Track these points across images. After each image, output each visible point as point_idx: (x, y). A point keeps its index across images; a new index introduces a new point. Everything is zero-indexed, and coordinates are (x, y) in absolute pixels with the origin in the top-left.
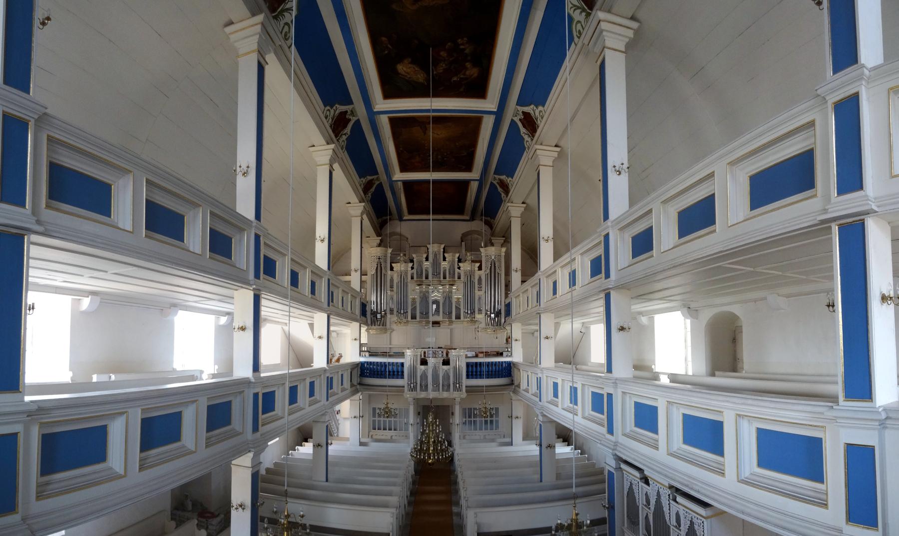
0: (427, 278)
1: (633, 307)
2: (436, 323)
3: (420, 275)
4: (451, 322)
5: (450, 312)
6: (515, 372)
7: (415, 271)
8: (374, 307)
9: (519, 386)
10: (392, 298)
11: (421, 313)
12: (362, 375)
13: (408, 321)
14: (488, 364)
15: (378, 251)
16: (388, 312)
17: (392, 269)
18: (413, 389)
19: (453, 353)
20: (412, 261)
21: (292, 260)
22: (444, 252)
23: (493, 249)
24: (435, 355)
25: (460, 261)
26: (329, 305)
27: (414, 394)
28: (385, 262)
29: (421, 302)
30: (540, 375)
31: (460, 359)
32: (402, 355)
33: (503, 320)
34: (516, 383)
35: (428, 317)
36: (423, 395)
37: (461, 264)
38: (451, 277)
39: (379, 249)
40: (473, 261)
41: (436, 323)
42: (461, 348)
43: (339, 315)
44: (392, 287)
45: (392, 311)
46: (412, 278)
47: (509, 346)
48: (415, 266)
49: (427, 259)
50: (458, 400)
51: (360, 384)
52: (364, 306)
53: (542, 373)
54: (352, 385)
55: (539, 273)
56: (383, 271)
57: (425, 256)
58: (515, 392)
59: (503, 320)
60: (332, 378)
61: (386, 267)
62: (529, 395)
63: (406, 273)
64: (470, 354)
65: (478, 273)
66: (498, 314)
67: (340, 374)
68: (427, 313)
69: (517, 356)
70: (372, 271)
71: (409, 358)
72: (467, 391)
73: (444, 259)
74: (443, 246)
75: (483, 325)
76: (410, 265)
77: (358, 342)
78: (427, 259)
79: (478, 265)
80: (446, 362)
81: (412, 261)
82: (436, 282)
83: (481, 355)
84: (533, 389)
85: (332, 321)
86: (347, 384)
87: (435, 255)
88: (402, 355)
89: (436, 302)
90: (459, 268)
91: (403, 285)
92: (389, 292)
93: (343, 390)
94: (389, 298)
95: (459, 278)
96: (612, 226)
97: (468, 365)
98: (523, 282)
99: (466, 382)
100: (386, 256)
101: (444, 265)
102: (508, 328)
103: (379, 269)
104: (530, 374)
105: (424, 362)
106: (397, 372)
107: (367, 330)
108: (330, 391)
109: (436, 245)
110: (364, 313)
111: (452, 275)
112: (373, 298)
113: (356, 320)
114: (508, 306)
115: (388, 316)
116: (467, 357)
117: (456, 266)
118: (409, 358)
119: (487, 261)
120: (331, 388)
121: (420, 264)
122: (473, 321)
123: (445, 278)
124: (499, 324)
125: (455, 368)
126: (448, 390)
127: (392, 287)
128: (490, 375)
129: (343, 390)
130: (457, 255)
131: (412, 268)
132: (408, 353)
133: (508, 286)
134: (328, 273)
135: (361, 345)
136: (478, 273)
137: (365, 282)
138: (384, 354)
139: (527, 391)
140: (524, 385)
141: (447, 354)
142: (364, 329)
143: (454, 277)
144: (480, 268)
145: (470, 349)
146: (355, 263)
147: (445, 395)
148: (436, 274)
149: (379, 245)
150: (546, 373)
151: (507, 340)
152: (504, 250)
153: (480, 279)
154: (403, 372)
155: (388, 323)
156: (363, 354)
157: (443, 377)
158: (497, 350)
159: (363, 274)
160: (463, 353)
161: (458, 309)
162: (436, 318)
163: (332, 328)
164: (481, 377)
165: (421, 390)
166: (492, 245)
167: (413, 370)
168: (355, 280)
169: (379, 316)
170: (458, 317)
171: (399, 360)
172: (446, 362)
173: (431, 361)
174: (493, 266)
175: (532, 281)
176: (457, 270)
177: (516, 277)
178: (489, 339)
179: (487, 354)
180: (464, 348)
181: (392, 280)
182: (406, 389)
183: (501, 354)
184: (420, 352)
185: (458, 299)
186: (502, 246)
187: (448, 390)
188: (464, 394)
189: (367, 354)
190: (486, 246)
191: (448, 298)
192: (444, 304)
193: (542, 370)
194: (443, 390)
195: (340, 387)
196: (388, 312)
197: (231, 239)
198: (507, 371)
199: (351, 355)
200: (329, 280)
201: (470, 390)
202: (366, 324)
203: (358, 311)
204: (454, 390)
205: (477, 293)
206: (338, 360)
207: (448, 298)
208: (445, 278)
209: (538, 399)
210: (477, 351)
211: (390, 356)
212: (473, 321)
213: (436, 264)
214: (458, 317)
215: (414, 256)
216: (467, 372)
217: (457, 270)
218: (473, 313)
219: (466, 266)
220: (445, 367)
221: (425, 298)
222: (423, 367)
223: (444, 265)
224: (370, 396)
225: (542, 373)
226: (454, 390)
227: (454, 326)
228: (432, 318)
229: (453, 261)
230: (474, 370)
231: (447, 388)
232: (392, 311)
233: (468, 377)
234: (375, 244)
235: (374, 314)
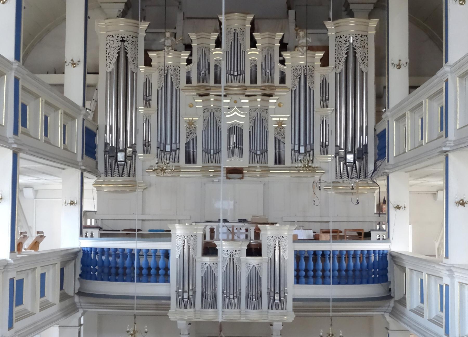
0: (218, 81)
1: (410, 182)
2: (235, 172)
3: (204, 75)
4: (266, 170)
5: (262, 149)
6: (393, 273)
7: (193, 67)
8: (111, 138)
9: (403, 301)
10: (147, 122)
11: (206, 151)
12: (86, 274)
13: (178, 169)
14: (340, 255)
15: (122, 26)
16: (140, 147)
17: (148, 62)
18: (185, 303)
19: (267, 232)
20: (188, 47)
21: (47, 103)
22: (253, 30)
23: (352, 22)
24: (232, 236)
25: (284, 47)
26: (16, 132)
27: (189, 313)
28: (135, 48)
29: (206, 129)
30: (446, 281)
31: (283, 243)
32: (166, 235)
33: (371, 167)
34: (397, 296)
35: (218, 160)
36: (209, 315)
37: (286, 55)
38: (265, 81)
39: (122, 22)
40: (310, 48)
41: (235, 172)
42: (285, 222)
43: (37, 153)
44: (147, 99)
45: (147, 146)
46: (189, 81)
47: (383, 218)
48: (195, 58)
49: (218, 44)
50: (278, 326)
51: (80, 293)
52: (90, 136)
53: (451, 276)
54: (64, 297)
55: (446, 68)
56: (131, 67)
57: (214, 37)
58: (395, 313)
59: (371, 167)
60: (20, 282)
61: (136, 58)
62: (424, 321)
63: (177, 70)
64: (303, 234)
65: (319, 73)
66: (361, 154)
67: (39, 272)
68: (218, 152)
69: (400, 240)
70: (106, 66)
71: (180, 241)
72: (296, 310)
73: (253, 44)
74: (250, 18)
75: (331, 176)
76: (185, 55)
77: (77, 209)
78: (218, 44)
79: (320, 55)
80: (254, 251)
81: (188, 47)
82: (236, 91)
83: (324, 237)
84: (433, 308)
85: (22, 164)
86: (53, 293)
87: (235, 36)
88: (166, 235)
89: (235, 130)
90: (282, 62)
91: (170, 97)
92: (141, 109)
93: (45, 306)
94: (141, 120)
95: (282, 81)
96: (452, 72)
97: (298, 256)
98: (412, 88)
99: (295, 291)
100: (136, 36)
101: (253, 55)
102: (382, 182)
103: (123, 63)
104: (425, 277)
105: (210, 250)
106: (157, 269)
107: (97, 185)
108: (16, 309)
109: (236, 16)
110: (90, 148)
111: (268, 74)
112: (111, 121)
113: (74, 164)
114: (382, 138)
115: (140, 155)
116: (296, 240)
117: (277, 58)
118: (180, 241)
119: (338, 47)
120: (20, 302)
121: (205, 55)
122: (309, 168)
123: (253, 81)
124: (362, 174)
125: (272, 262)
126: (258, 305)
127: (147, 99)
128: (343, 278)
129: (45, 306)
130: (279, 36)
131: (189, 62)
132: (179, 231)
133: (381, 98)
134: (16, 65)
135: (83, 214)
136: (319, 73)
137: (94, 87)
138: (129, 234)
139: (419, 312)
140: (413, 301)
141: (257, 235)
142: (90, 181)
143: (271, 79)
144: (325, 62)
145: (303, 224)
146: (74, 48)
147: (253, 315)
148: (236, 71)
149: (124, 14)
150: (459, 277)
151: (379, 207)
152: (373, 23)
153: (324, 84)
154: (167, 269)
155: (139, 171)
156: (89, 231)
157: (249, 280)
158: (358, 227)
159: (90, 70)
160: (287, 231)
161: (279, 143)
162: (236, 162)
163: (22, 180)
164: (324, 280)
165: (204, 305)
166: (351, 14)
167: (189, 264)
168: (73, 81)
169: (121, 156)
170: (280, 160)
171: (161, 245)
172: (254, 251)
173: (224, 247)
174: (351, 58)
175: (432, 85)
176: (278, 66)
177: (398, 80)
178: (344, 208)
179: (337, 236)
180: (292, 223)
181: (147, 85)
182: (173, 302)
183: (367, 236)
184: (200, 229)
185: (280, 123)
186: (371, 16)
187: (258, 305)
188: (289, 316)
189: (96, 232)
190: (336, 17)
191: (259, 121)
192: (251, 133)
193: (450, 270)
194: (248, 307)
195: (38, 300)
196: (140, 147)
197: (26, 106)
198: (380, 270)
199: (66, 235)
200: (17, 81)
201: (302, 306)
202: (94, 171)
203: (77, 145)
204: (270, 306)
205: (319, 113)
206: (35, 245)
207: (259, 121)
208: (253, 81)
209: (442, 331)
210: (318, 228)
211: (143, 237)
212: (309, 168)
213: (236, 56)
214: (280, 160)
215: (193, 37)
216: (297, 270)
217: (278, 66)
218: (310, 151)
219: (296, 59)
220: (254, 260)
221: (213, 120)
222: (208, 260)
223: (253, 55)
224: (100, 317)
225: (451, 276)
226: (270, 306)
227: (271, 177)
228: (228, 162)
229: (271, 48)
230: (310, 267)
231: (254, 301)
232: (147, 146)
233: (298, 280)
234: (116, 13)
235: (111, 152)
